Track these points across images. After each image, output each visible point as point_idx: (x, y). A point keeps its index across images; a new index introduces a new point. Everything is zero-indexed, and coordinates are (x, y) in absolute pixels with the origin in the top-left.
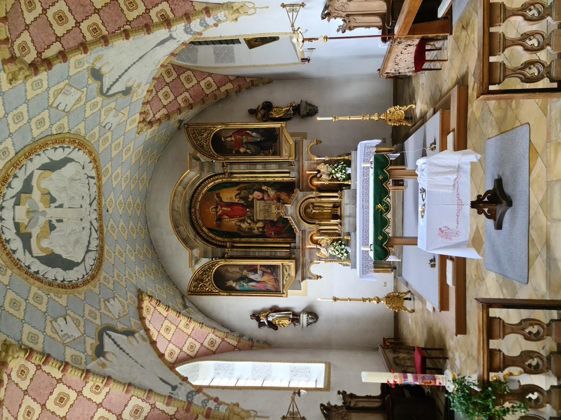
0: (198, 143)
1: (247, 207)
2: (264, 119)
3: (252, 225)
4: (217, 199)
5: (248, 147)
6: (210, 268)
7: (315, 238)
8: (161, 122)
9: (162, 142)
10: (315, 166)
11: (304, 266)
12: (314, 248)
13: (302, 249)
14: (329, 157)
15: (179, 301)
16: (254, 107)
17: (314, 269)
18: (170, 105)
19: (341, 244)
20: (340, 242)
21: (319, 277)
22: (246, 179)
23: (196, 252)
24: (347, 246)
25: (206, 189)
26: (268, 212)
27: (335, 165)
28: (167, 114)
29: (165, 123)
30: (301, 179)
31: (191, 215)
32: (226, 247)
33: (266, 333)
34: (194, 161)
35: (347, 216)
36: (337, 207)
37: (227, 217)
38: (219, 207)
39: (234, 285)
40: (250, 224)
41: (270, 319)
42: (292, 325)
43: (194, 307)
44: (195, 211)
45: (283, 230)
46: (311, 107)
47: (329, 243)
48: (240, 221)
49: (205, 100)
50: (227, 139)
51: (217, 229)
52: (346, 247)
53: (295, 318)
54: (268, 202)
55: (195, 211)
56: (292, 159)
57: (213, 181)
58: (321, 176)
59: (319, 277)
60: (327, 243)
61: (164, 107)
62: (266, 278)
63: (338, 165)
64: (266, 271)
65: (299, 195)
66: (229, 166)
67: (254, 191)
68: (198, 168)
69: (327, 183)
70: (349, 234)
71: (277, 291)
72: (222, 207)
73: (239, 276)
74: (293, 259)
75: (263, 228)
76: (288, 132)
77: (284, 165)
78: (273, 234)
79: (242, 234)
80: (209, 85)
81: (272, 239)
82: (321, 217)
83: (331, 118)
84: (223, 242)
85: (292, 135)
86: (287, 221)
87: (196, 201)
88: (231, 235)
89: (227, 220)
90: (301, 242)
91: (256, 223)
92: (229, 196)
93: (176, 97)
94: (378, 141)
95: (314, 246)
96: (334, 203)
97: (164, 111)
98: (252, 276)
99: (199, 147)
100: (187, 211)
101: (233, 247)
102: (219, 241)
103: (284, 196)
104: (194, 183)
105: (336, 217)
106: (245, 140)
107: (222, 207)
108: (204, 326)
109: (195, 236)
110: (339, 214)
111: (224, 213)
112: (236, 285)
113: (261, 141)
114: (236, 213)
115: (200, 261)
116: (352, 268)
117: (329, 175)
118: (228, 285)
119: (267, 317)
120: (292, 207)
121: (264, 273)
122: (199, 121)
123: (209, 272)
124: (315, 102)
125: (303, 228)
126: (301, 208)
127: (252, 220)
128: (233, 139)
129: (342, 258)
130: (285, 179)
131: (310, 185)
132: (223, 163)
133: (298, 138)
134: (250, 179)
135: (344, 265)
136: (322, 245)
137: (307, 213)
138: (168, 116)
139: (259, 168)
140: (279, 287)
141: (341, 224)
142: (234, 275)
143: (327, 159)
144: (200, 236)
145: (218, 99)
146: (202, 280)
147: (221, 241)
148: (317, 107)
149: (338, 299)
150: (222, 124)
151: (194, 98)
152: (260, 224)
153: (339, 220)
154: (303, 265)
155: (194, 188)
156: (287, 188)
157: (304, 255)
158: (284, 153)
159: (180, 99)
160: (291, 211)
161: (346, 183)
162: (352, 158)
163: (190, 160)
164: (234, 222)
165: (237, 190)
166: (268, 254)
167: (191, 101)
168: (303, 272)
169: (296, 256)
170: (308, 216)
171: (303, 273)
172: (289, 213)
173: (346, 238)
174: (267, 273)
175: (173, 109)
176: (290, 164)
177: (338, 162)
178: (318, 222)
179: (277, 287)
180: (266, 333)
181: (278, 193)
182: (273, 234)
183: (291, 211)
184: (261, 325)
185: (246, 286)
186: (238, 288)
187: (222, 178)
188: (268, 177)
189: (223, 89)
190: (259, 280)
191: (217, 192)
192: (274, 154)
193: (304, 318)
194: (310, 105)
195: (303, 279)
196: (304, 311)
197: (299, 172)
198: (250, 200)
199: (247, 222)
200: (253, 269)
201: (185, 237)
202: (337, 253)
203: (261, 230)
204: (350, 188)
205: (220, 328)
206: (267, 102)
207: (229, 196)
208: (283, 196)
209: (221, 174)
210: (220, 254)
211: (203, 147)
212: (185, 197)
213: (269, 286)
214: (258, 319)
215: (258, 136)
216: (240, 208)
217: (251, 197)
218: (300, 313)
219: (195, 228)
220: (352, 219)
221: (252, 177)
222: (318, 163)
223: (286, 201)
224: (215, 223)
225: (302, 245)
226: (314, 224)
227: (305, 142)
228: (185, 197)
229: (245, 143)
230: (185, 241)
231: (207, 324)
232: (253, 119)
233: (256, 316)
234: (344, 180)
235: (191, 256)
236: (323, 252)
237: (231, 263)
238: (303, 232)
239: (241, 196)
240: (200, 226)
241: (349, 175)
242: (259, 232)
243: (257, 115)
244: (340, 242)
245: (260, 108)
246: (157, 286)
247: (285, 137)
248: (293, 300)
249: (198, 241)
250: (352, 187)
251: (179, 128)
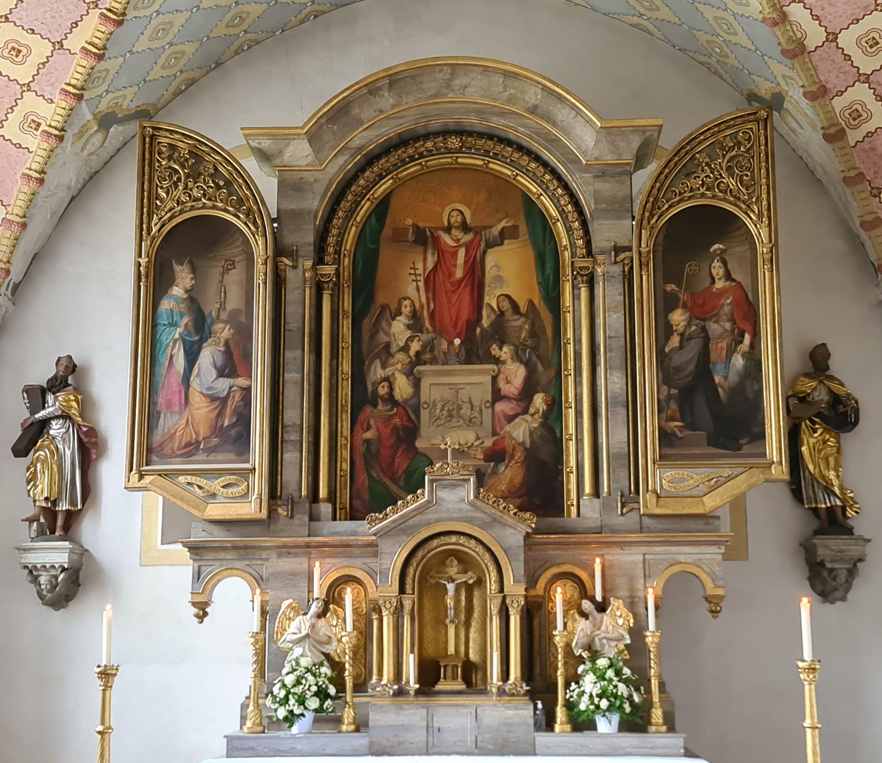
0: (702, 158)
1: (468, 338)
2: (793, 401)
3: (401, 356)
4: (496, 231)
5: (690, 338)
6: (241, 202)
7: (349, 595)
8: (775, 24)
9: (703, 37)
10: (624, 593)
11: (244, 551)
12: (310, 591)
13: (308, 546)
14: (658, 646)
15: (129, 99)
16: (836, 366)
17: (235, 596)
18: (840, 58)
19: (322, 694)
20: (332, 690)
21: (202, 610)
22: (570, 334)
23: (299, 153)
24: (316, 721)
25: (534, 188)
26: (450, 416)
27: (627, 671)
28: (804, 47)
29: (771, 40)
30: (573, 538)
31: (437, 134)
32: (320, 260)
34: (636, 142)
35: (429, 718)
36: (467, 680)
37: (430, 265)
38: (468, 237)
39: (177, 291)
40: (405, 349)
41: (56, 428)
42: (31, 512)
43: (105, 156)
44: (449, 151)
45: (383, 470)
46: (843, 576)
47: (330, 649)
48: (415, 315)
49: (860, 187)
50: (716, 264)
51: (387, 231)
52: (310, 716)
53: (58, 521)
54: (487, 414)
55: (449, 151)
56: (648, 503)
57: (562, 212)
58: (585, 615)
59: (202, 610)
60: (329, 641)
61: (832, 37)
62: (201, 410)
63: (627, 682)
64: (228, 411)
65: (512, 532)
66: (616, 269)
67: (527, 364)
68: (610, 159)
69: (559, 640)
71: (146, 452)
72: (468, 246)
73: (211, 308)
74: (271, 511)
75: (390, 399)
76: (749, 487)
77: (623, 474)
78: (369, 435)
79: (367, 324)
81: (347, 432)
83: (807, 654)
84: (338, 252)
85: (738, 505)
86: (414, 485)
87: (487, 153)
88: (365, 282)
89: (420, 266)
90: (337, 539)
91: (409, 373)
92: (509, 272)
93: (867, 79)
95: (318, 592)
96: (482, 667)
97: (815, 36)
98: (208, 357)
99: (683, 162)
100: (450, 121)
101: (319, 289)
102: (341, 235)
103: (509, 473)
104: (553, 142)
105: (430, 675)
106: (714, 328)
107: (468, 246)
108: (33, 185)
109: (360, 149)
110: (440, 686)
111: (444, 257)
112: (176, 299)
113: (714, 387)
114: (444, 299)
115: (267, 169)
116: (230, 739)
117: (589, 647)
118: (177, 268)
119: (65, 416)
120: (465, 506)
121: (220, 401)
122: (781, 170)
123: (226, 201)
124: (860, 591)
125: (385, 546)
126: (462, 540)
127: (418, 359)
128: (719, 284)
129: (269, 702)
130: (573, 478)
131: (549, 574)
132: (629, 249)
133: (725, 527)
134: (571, 349)
135: (244, 707)
136: (322, 622)
137: (443, 563)
138: (797, 51)
139: (612, 382)
140: (165, 458)
141: (401, 693)
142: (212, 290)
143: (651, 638)
144: (361, 169)
145: (864, 235)
147: (339, 244)
148: (844, 599)
149: (107, 687)
150: (774, 246)
151: (866, 145)
152: (403, 388)
153: (414, 686)
154: (246, 548)
155: (535, 146)
156: (540, 491)
157: (285, 550)
158: (669, 473)
159: (861, 93)
160: (450, 501)
161: (560, 713)
162: (658, 737)
163: (636, 129)
164: (413, 291)
165: (531, 303)
166: (290, 415)
167: (853, 136)
168: (221, 548)
169: (282, 521)
170: (430, 568)
171: (214, 550)
172: (443, 494)
173: (348, 715)
174: (220, 415)
175: (822, 67)
176: (629, 498)
177: (640, 682)
178: (407, 604)
179: (167, 450)
181: (519, 455)
182: (369, 435)
184: (36, 396)
185: (172, 340)
186: (166, 305)
187: (573, 245)
188: (579, 413)
190: (195, 384)
191: (523, 229)
192: (665, 438)
193: (55, 554)
194: (852, 572)
195: (195, 549)
197: (599, 531)
198: (495, 350)
199: (410, 339)
201: (355, 111)
202: (289, 680)
203: (383, 390)
204: (538, 728)
205: (29, 243)
206: (857, 411)
207: (509, 272)
208: (510, 474)
209: (588, 243)
210: (289, 239)
211: (687, 175)
212: (502, 114)
213: (170, 423)
214: (57, 384)
215: (733, 378)
216: (465, 314)
217: (505, 353)
218: (71, 541)
219: (387, 149)
220: (420, 737)
221: (578, 355)
222: (633, 604)
223: (490, 482)
224: (409, 222)
225: (324, 545)
226: (402, 590)
227: (713, 554)
228: (502, 114)
229: (704, 329)
230: (339, 114)
231: (39, 199)
232: (796, 362)
233: (69, 376)
234: (570, 706)
235: (283, 136)
236: (293, 626)
237: (258, 279)
238: (372, 549)
239: (509, 315)
240: (396, 167)
241: (591, 726)
242: (376, 384)
243: (806, 375)
244: (332, 690)
245: (835, 387)
246: (181, 19)
247: (730, 478)
248: (126, 516)
249: (341, 160)
250: (542, 738)
251: (752, 97)
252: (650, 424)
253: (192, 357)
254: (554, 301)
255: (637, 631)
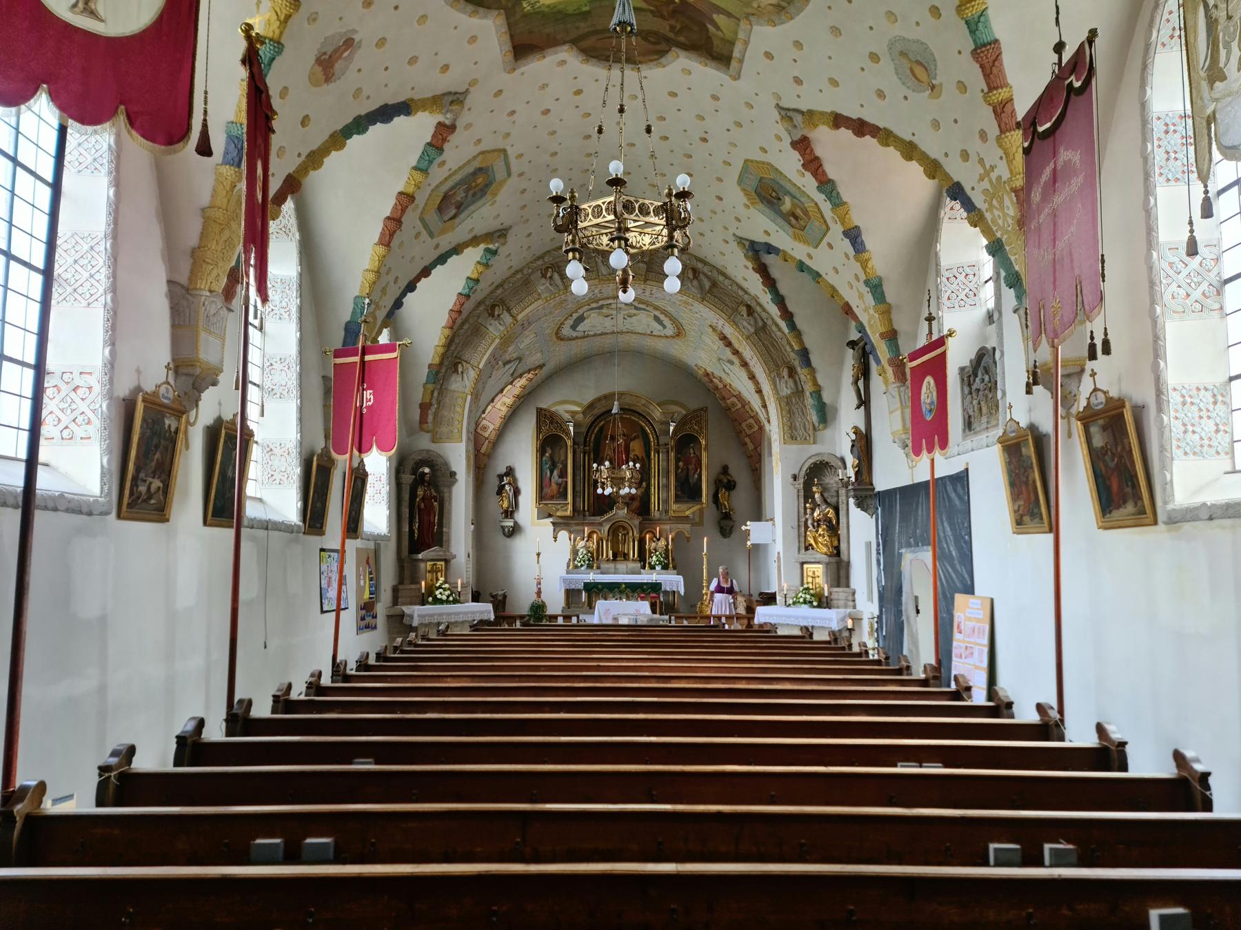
16: (731, 471)
17: (563, 535)
21: (555, 538)
33: (493, 483)
41: (507, 487)
53: (509, 513)
56: (671, 513)
59: (555, 538)
62: (554, 487)
65: (636, 521)
70: (598, 568)
71: (541, 496)
73: (556, 459)
80: (750, 427)
82: (615, 544)
94: (682, 592)
98: (555, 473)
105: (615, 556)
119: (509, 483)
121: (559, 485)
139: (663, 481)
146: (551, 423)
157: (577, 524)
162: (671, 571)
176: (667, 512)
177: (667, 557)
180: (493, 483)
183: (621, 513)
184: (501, 477)
189: (747, 440)
192: (676, 496)
196: (516, 523)
200: (563, 474)
208: (636, 504)
213: (546, 490)
214: (507, 474)
227: (688, 526)
232: (717, 469)
233: (510, 472)
238: (601, 524)
252: (673, 492)
253: (552, 473)
254: (649, 456)
255: (667, 546)
